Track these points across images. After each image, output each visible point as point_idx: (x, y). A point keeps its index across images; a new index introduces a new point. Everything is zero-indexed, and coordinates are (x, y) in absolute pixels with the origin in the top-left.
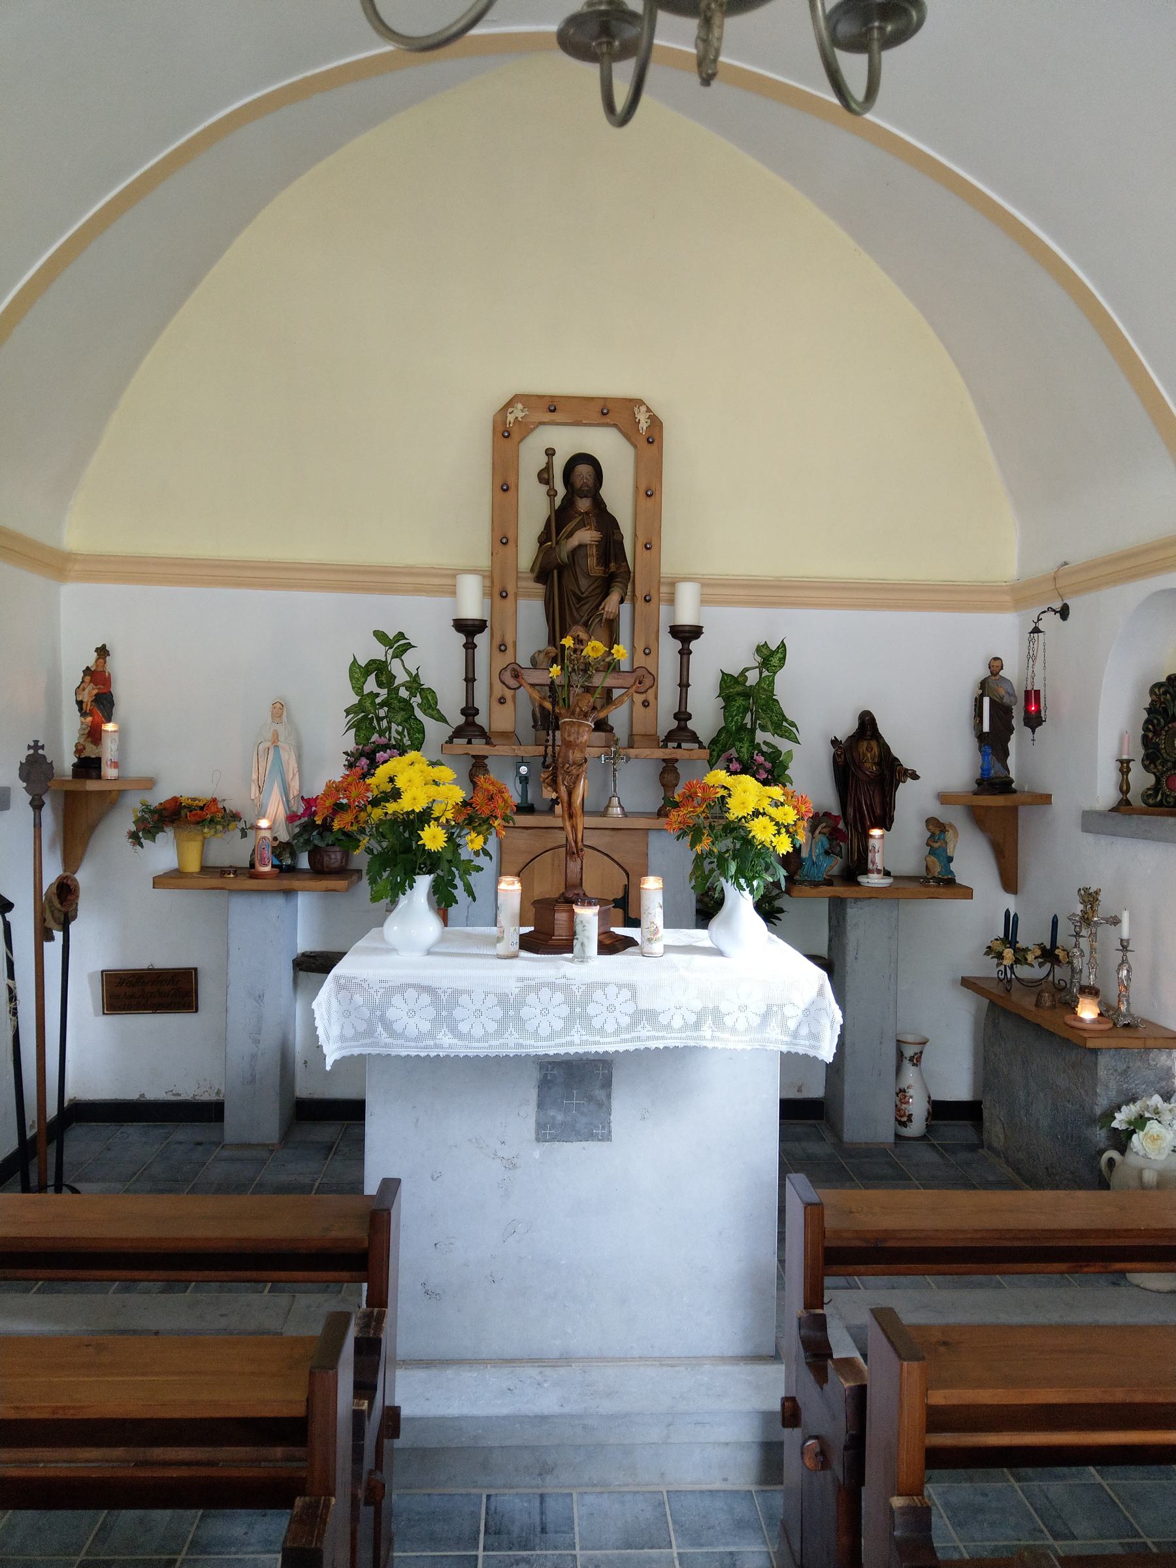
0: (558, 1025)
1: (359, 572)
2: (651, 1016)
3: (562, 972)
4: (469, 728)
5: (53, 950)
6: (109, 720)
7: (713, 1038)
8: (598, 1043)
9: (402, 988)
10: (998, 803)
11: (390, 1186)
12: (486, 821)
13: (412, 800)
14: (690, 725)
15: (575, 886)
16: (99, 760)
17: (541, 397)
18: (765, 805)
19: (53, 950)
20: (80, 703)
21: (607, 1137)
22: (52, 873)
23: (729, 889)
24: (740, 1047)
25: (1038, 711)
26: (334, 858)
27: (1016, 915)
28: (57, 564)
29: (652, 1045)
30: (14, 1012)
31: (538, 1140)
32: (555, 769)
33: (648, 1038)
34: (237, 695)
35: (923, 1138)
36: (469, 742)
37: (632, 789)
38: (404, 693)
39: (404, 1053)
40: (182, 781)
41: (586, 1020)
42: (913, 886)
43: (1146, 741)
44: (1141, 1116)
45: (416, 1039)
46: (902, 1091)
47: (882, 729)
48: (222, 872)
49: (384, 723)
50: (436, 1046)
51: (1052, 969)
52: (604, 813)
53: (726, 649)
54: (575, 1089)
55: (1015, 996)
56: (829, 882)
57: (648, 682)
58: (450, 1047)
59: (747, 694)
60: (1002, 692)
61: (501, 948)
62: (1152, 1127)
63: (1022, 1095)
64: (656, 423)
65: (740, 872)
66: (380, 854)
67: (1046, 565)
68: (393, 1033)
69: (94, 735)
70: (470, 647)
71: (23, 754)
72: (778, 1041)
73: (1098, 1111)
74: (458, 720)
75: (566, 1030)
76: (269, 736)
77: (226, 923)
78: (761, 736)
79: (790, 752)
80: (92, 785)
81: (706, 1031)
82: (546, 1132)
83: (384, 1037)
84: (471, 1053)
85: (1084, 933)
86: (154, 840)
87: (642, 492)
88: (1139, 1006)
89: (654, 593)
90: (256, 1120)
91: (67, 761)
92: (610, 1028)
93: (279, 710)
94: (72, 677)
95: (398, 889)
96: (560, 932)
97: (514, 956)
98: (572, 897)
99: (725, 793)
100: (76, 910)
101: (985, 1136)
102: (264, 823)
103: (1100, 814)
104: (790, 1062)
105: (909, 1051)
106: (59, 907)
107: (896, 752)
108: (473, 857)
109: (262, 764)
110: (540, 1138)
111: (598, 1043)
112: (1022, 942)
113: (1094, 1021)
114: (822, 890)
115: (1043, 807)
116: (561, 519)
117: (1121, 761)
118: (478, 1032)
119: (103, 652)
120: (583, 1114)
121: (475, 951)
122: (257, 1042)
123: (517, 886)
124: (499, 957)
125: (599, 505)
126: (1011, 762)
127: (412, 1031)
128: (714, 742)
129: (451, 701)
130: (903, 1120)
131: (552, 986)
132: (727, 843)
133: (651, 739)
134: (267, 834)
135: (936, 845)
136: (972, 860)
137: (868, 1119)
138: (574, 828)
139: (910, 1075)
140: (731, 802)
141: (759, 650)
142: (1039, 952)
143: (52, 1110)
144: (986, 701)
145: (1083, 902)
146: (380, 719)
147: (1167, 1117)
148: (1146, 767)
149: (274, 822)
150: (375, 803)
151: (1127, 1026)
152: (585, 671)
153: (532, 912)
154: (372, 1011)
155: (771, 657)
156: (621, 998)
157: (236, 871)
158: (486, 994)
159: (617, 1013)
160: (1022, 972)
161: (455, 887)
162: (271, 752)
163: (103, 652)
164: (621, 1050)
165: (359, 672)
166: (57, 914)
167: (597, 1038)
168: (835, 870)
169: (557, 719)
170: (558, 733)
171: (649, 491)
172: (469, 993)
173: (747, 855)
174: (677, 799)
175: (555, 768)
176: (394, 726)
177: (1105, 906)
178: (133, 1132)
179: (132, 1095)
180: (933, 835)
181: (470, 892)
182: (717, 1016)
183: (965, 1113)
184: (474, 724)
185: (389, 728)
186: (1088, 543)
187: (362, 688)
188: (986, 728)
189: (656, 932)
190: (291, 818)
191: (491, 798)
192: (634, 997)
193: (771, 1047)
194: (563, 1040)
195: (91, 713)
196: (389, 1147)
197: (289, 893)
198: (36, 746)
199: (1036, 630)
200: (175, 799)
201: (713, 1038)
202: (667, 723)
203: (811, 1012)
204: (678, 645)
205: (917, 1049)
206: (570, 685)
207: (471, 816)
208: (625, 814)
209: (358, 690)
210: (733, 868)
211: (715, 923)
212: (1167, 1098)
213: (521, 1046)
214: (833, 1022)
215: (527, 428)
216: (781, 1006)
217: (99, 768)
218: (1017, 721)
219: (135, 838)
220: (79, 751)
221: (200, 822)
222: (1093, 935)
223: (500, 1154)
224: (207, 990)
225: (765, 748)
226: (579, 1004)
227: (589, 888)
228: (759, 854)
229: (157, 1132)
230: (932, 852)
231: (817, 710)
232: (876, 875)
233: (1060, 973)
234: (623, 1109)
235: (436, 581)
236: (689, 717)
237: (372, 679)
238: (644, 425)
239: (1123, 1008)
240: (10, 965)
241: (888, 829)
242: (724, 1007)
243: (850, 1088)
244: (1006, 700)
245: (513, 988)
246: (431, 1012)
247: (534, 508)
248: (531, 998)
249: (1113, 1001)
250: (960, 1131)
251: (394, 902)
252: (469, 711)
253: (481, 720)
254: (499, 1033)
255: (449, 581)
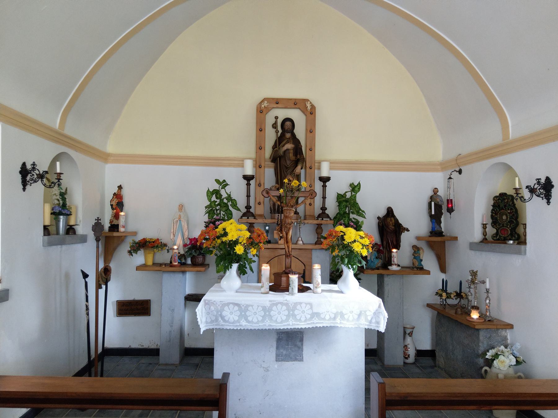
0: (284, 318)
1: (210, 159)
2: (317, 315)
3: (285, 299)
4: (248, 213)
5: (102, 292)
6: (122, 211)
7: (341, 323)
8: (299, 325)
9: (228, 304)
10: (438, 240)
11: (226, 376)
12: (257, 244)
13: (232, 236)
14: (326, 212)
15: (288, 268)
16: (118, 225)
17: (273, 99)
18: (358, 238)
19: (102, 292)
20: (112, 205)
21: (302, 360)
22: (101, 266)
23: (345, 268)
24: (350, 326)
25: (452, 207)
26: (200, 259)
27: (446, 281)
28: (105, 157)
29: (318, 325)
30: (88, 314)
31: (276, 361)
32: (281, 226)
33: (317, 323)
34: (166, 201)
35: (414, 363)
36: (248, 218)
37: (305, 235)
38: (225, 201)
39: (228, 328)
40: (147, 232)
41: (294, 316)
42: (408, 270)
43: (492, 217)
44: (497, 354)
45: (233, 323)
46: (406, 346)
47: (396, 213)
48: (161, 265)
49: (218, 212)
50: (240, 326)
51: (460, 300)
52: (296, 244)
53: (339, 184)
54: (290, 342)
55: (447, 310)
56: (378, 269)
57: (314, 195)
58: (245, 326)
59: (347, 201)
60: (438, 200)
61: (263, 290)
62: (501, 358)
63: (451, 347)
64: (313, 107)
65: (349, 262)
66: (220, 256)
67: (453, 155)
68: (225, 321)
69: (117, 216)
70: (248, 185)
71: (93, 222)
72: (364, 324)
73: (480, 352)
74: (244, 210)
75: (287, 320)
76: (178, 217)
77: (162, 283)
78: (352, 216)
79: (362, 222)
80: (115, 234)
81: (338, 320)
82: (279, 358)
83: (222, 322)
84: (252, 328)
85: (472, 286)
86: (137, 253)
87: (258, 166)
88: (494, 313)
89: (313, 166)
90: (171, 355)
91: (107, 226)
92: (303, 319)
93: (181, 207)
94: (109, 196)
95: (227, 268)
96: (284, 284)
97: (267, 293)
98: (287, 272)
99: (343, 234)
100: (110, 278)
101: (437, 362)
102: (175, 247)
103: (476, 243)
104: (368, 332)
105: (408, 331)
106: (104, 276)
107: (400, 222)
108: (252, 257)
109: (175, 227)
110: (277, 360)
111: (299, 325)
112: (449, 291)
113: (477, 319)
114: (377, 270)
115: (454, 241)
116: (280, 141)
117: (483, 224)
118: (255, 320)
119: (120, 187)
120: (293, 351)
121: (253, 291)
122: (171, 326)
123: (269, 268)
124: (262, 293)
125: (293, 135)
126: (442, 225)
127: (231, 320)
128: (335, 218)
129: (242, 203)
130: (406, 357)
131: (282, 303)
132: (343, 253)
133: (312, 217)
134: (177, 251)
135: (416, 255)
136: (429, 261)
137: (393, 357)
138: (288, 247)
139: (409, 340)
140: (345, 237)
141: (351, 185)
142: (455, 294)
143: (100, 350)
144: (433, 203)
145: (472, 275)
146: (217, 210)
147: (506, 354)
148: (492, 226)
149: (179, 247)
150: (218, 237)
151: (489, 321)
152: (292, 191)
153: (273, 277)
154: (217, 312)
155: (355, 188)
156: (307, 308)
157: (166, 265)
158: (258, 306)
159: (305, 314)
160: (450, 301)
161: (246, 268)
162: (178, 222)
163: (120, 187)
164: (307, 327)
165: (210, 194)
166: (103, 279)
167: (298, 323)
168: (379, 265)
169: (282, 208)
170: (282, 215)
171: (311, 130)
172: (252, 306)
173: (350, 256)
174: (326, 236)
175: (282, 225)
176: (222, 212)
177: (480, 277)
178: (126, 360)
179: (127, 346)
180: (415, 251)
181: (251, 269)
182: (342, 315)
183: (430, 354)
184: (250, 212)
185: (220, 213)
186: (467, 148)
187: (211, 199)
188: (433, 213)
189: (318, 284)
190: (185, 245)
191: (259, 236)
192: (311, 308)
193: (362, 326)
194: (286, 324)
195: (116, 209)
196: (221, 365)
197: (184, 272)
198: (98, 219)
199: (450, 178)
200: (144, 239)
201: (341, 323)
202: (318, 211)
203: (377, 314)
204: (322, 184)
205: (411, 330)
206: (286, 196)
207: (251, 243)
208: (304, 244)
209: (210, 200)
210: (346, 261)
211: (339, 282)
212: (506, 347)
213: (271, 326)
214: (384, 317)
215: (268, 109)
216: (365, 312)
217: (118, 228)
218: (444, 210)
219: (130, 252)
220: (111, 222)
221: (153, 247)
222: (475, 288)
223: (263, 366)
224: (154, 308)
225: (353, 220)
226: (291, 309)
227: (293, 268)
228: (356, 256)
229: (135, 359)
230: (415, 258)
231: (372, 205)
232: (395, 266)
233: (463, 302)
234: (307, 350)
235: (236, 162)
236: (326, 209)
237: (214, 196)
238: (309, 108)
239: (488, 314)
240: (87, 297)
241: (398, 249)
242: (344, 312)
243: (387, 344)
244: (440, 203)
245: (268, 304)
246: (238, 313)
247: (271, 137)
248: (274, 308)
249: (484, 312)
250: (427, 361)
251: (225, 273)
252: (248, 207)
253: (252, 210)
254: (263, 321)
255: (241, 162)
